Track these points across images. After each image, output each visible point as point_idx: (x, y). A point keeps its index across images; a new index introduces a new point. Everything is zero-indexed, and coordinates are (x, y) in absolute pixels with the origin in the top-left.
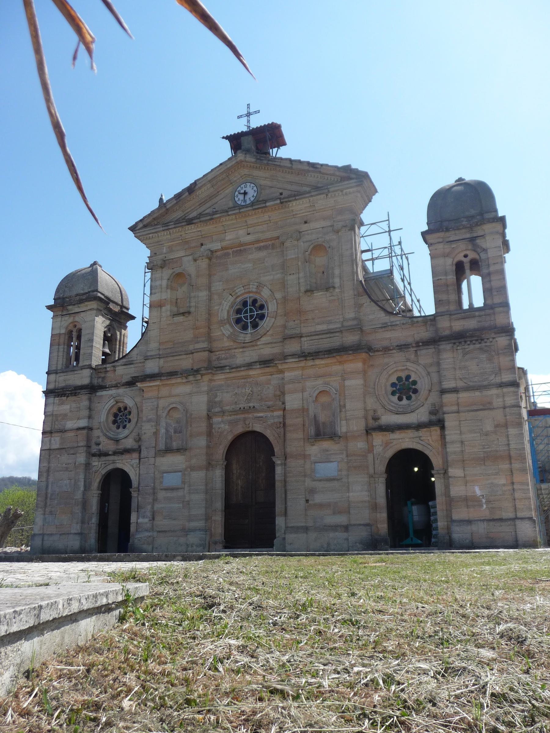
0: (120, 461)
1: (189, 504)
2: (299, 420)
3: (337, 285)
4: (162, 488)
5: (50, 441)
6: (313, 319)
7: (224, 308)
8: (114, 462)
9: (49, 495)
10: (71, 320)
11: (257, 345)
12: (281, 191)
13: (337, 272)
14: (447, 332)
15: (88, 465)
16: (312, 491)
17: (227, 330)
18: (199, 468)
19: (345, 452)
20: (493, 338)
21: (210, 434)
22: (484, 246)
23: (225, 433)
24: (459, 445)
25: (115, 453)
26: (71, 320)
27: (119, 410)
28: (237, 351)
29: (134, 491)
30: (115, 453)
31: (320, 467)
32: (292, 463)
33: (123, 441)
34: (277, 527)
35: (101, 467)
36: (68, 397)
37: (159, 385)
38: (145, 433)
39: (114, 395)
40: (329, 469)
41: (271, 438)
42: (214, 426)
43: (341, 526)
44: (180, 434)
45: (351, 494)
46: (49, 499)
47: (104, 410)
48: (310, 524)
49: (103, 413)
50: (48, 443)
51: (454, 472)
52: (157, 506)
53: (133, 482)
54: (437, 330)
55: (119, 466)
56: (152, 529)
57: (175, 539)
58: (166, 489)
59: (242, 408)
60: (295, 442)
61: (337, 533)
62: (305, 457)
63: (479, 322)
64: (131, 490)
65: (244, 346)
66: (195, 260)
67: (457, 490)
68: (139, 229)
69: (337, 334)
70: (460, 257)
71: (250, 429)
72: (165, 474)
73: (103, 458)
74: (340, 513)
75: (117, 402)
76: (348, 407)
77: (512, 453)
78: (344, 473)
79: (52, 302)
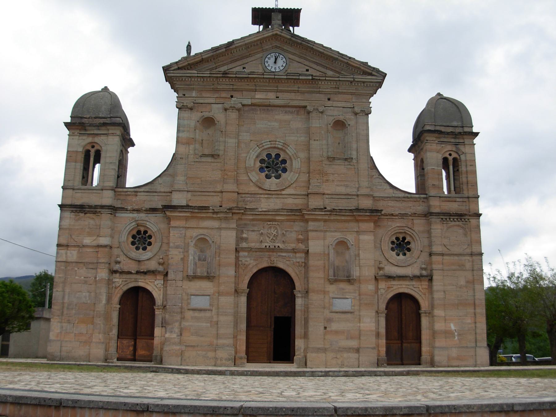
0: (143, 280)
1: (217, 324)
2: (320, 263)
3: (354, 157)
4: (190, 308)
5: (66, 254)
6: (333, 181)
7: (252, 160)
8: (136, 280)
9: (66, 305)
10: (90, 139)
11: (281, 194)
12: (307, 68)
13: (354, 146)
14: (437, 210)
15: (109, 282)
16: (329, 320)
17: (255, 176)
18: (227, 294)
19: (357, 292)
20: (468, 219)
21: (237, 265)
22: (463, 150)
23: (251, 266)
24: (443, 293)
25: (138, 272)
26: (90, 139)
27: (139, 232)
28: (262, 196)
29: (158, 309)
30: (138, 272)
31: (337, 302)
32: (313, 297)
33: (145, 262)
34: (296, 348)
35: (122, 284)
36: (85, 214)
37: (188, 217)
38: (172, 258)
39: (137, 219)
40: (344, 304)
41: (293, 275)
42: (240, 259)
43: (353, 349)
44: (204, 262)
45: (362, 325)
46: (65, 309)
47: (125, 231)
48: (327, 346)
49: (124, 233)
50: (64, 255)
51: (438, 312)
52: (185, 324)
53: (156, 300)
54: (429, 207)
55: (141, 284)
56: (180, 343)
57: (204, 353)
58: (194, 310)
59: (268, 247)
60: (317, 279)
61: (350, 354)
62: (325, 293)
63: (459, 206)
64: (155, 307)
65: (269, 193)
66: (226, 110)
67: (439, 326)
68: (173, 70)
69: (354, 197)
70: (447, 155)
71: (274, 265)
72: (193, 297)
73: (125, 276)
74: (352, 338)
75: (138, 226)
76: (362, 256)
77: (477, 302)
78: (357, 308)
79: (69, 120)
